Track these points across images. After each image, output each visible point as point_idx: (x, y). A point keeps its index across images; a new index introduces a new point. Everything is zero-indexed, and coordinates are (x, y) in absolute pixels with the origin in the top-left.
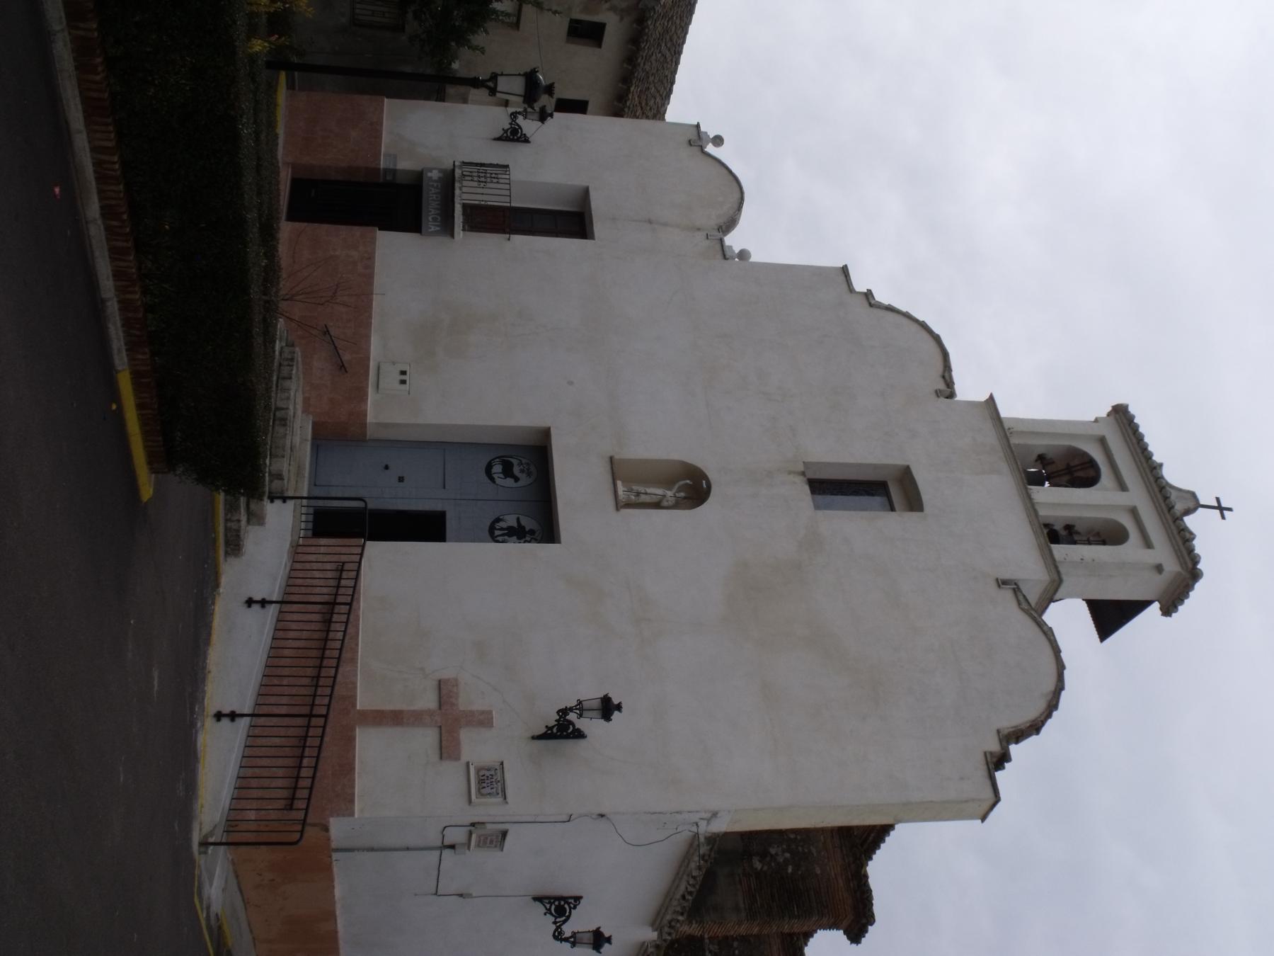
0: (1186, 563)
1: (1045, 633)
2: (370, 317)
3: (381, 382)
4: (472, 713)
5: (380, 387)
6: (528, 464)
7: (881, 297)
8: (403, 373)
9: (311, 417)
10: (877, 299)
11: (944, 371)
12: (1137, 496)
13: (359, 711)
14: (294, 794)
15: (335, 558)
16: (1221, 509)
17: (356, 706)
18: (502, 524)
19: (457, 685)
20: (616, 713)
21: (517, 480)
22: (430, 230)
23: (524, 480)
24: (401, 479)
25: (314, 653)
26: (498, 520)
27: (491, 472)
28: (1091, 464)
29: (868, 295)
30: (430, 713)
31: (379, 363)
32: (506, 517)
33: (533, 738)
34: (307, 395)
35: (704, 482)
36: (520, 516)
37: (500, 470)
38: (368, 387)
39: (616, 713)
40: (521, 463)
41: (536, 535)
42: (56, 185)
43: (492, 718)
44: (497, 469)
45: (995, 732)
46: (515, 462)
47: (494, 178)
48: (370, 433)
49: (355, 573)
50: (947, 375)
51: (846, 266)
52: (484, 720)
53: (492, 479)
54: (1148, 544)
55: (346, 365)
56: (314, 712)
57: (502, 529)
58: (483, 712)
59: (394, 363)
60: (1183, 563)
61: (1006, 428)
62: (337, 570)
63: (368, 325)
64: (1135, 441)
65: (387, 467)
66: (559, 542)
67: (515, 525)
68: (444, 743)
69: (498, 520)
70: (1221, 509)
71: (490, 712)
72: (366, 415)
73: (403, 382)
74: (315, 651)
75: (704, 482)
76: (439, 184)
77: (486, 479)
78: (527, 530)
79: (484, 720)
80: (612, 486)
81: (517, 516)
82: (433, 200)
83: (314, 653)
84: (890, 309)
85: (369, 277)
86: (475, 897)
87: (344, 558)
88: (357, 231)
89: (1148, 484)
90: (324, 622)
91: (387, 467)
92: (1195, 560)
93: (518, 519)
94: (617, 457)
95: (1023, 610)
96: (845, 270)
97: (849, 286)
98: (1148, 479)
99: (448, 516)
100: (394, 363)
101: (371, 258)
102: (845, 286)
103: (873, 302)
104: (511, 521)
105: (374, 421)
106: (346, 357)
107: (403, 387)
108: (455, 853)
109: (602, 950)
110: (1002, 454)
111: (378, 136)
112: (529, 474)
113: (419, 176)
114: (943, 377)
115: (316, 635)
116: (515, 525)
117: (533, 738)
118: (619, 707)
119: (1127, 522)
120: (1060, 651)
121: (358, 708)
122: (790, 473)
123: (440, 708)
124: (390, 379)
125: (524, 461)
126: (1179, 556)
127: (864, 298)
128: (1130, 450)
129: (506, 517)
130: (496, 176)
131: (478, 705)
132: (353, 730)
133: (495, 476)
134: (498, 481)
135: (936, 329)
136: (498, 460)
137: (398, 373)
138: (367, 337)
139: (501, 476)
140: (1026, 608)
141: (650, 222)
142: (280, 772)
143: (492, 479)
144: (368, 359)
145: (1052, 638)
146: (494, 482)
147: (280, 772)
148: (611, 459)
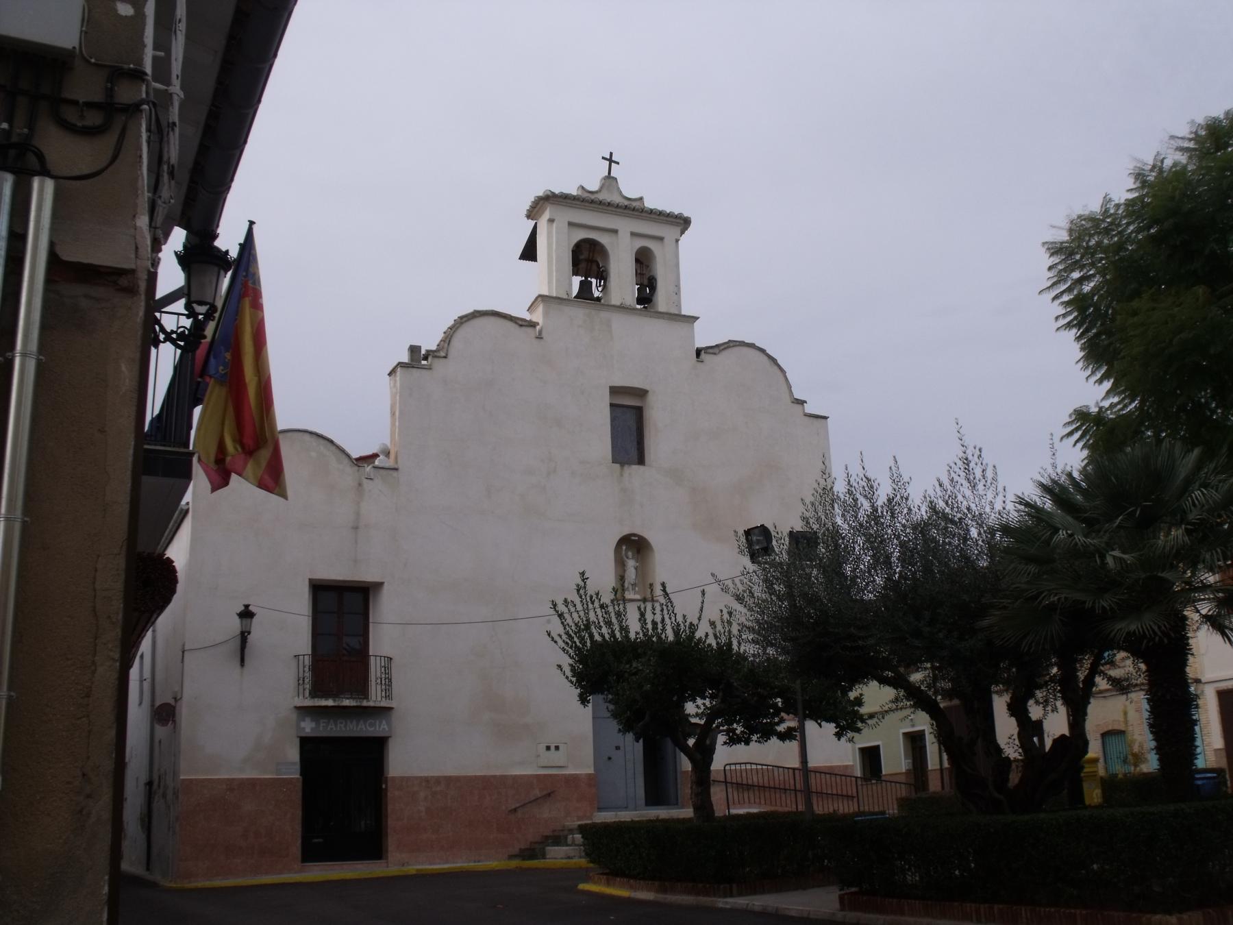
2: (495, 777)
3: (558, 765)
8: (548, 748)
9: (595, 814)
11: (516, 323)
12: (625, 226)
14: (845, 796)
20: (250, 608)
22: (387, 729)
24: (618, 748)
25: (767, 794)
34: (575, 819)
39: (250, 608)
42: (185, 344)
45: (792, 404)
47: (304, 681)
49: (897, 784)
50: (520, 323)
55: (545, 792)
56: (797, 792)
57: (1110, 679)
59: (539, 756)
62: (785, 793)
65: (610, 758)
72: (590, 774)
73: (557, 748)
74: (766, 793)
76: (322, 721)
82: (345, 726)
83: (767, 794)
85: (450, 780)
86: (1206, 683)
88: (392, 794)
89: (614, 213)
90: (748, 790)
95: (719, 353)
101: (427, 780)
105: (592, 768)
106: (537, 793)
107: (560, 748)
108: (390, 737)
109: (298, 739)
111: (252, 783)
113: (305, 742)
114: (521, 326)
115: (757, 793)
122: (622, 475)
126: (672, 223)
128: (582, 208)
130: (301, 679)
135: (470, 310)
137: (548, 752)
138: (515, 778)
141: (356, 528)
142: (741, 795)
144: (538, 776)
145: (738, 343)
147: (741, 795)
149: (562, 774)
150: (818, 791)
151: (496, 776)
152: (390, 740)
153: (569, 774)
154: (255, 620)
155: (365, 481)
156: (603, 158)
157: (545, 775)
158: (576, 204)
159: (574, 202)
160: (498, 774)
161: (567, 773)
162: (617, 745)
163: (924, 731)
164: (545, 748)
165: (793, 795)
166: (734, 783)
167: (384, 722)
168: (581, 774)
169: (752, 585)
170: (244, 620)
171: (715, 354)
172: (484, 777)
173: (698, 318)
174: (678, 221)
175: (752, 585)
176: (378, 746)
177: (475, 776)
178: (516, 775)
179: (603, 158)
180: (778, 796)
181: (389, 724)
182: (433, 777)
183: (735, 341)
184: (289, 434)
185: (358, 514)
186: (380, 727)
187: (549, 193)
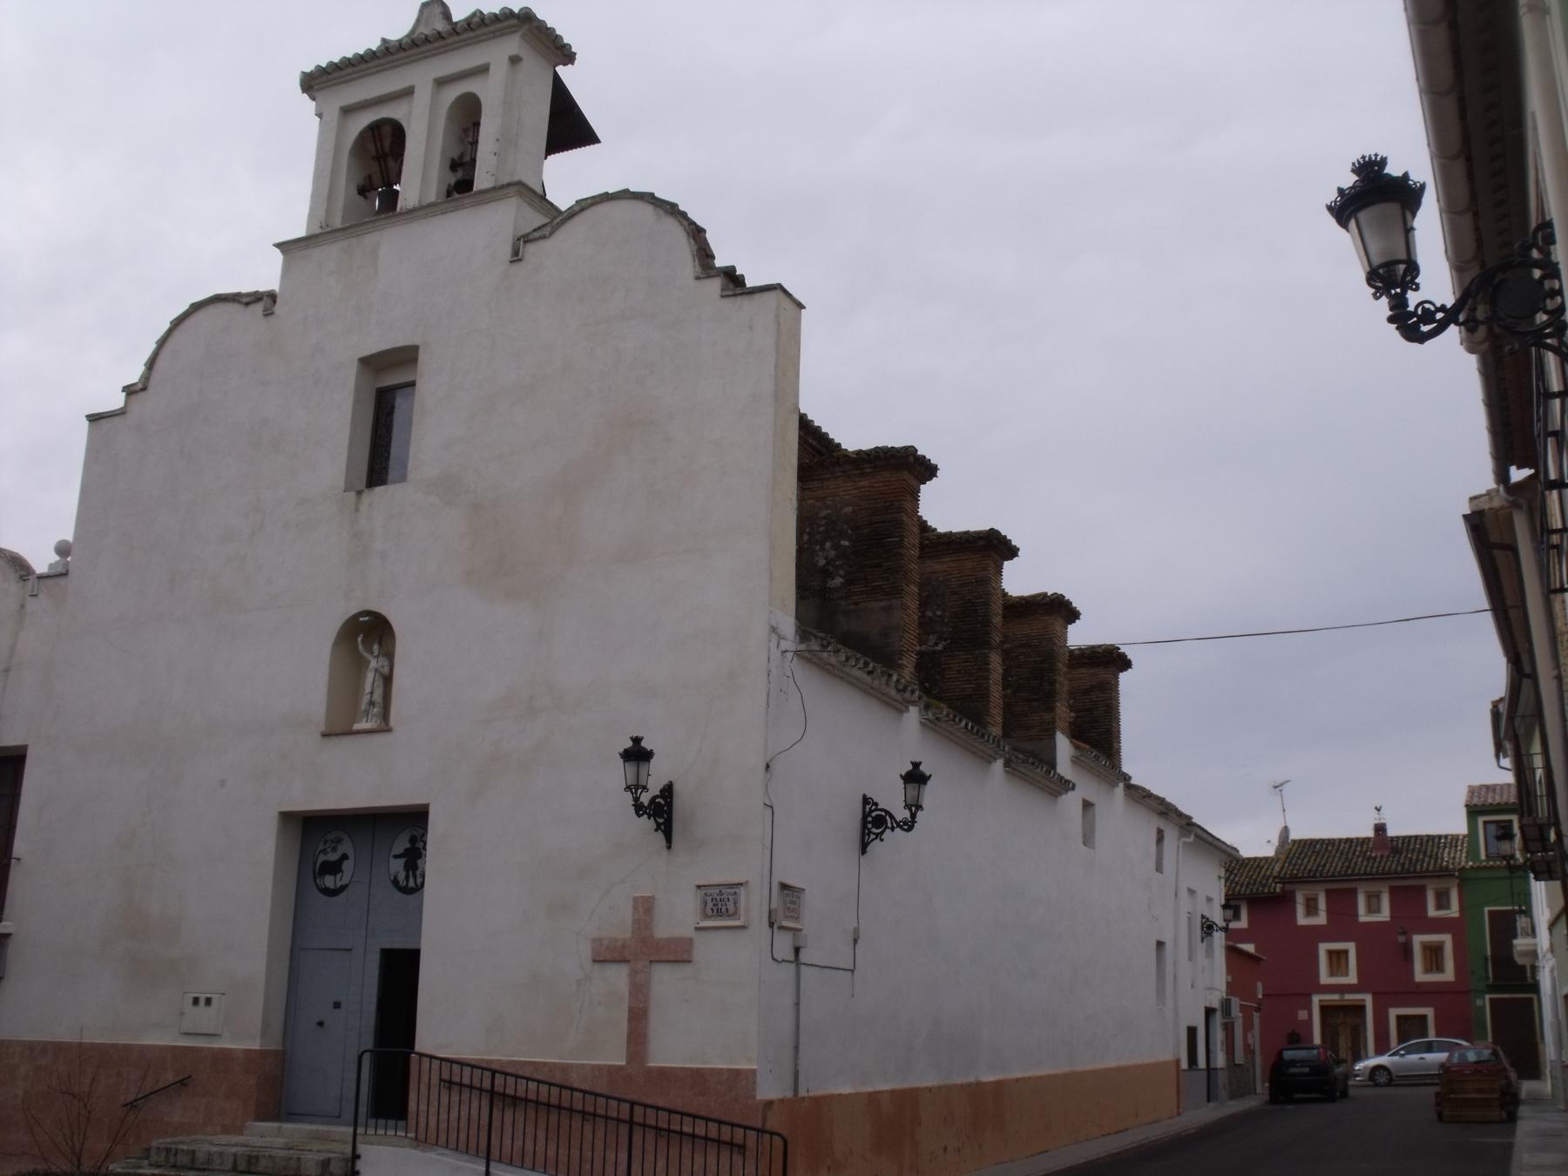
1: (583, 210)
2: (115, 1046)
4: (636, 922)
5: (211, 1032)
6: (325, 842)
7: (134, 375)
8: (196, 1001)
11: (239, 302)
12: (421, 76)
13: (627, 1063)
14: (726, 1143)
15: (435, 1091)
18: (402, 877)
19: (600, 940)
20: (643, 744)
21: (344, 857)
23: (346, 847)
24: (337, 1005)
25: (553, 1118)
26: (395, 882)
27: (334, 890)
28: (375, 129)
29: (130, 391)
30: (633, 974)
31: (180, 1033)
32: (393, 871)
33: (669, 847)
35: (361, 619)
36: (392, 854)
37: (332, 878)
38: (213, 1048)
39: (643, 744)
40: (324, 851)
43: (643, 897)
44: (329, 881)
46: (322, 858)
48: (274, 1045)
50: (245, 300)
52: (645, 907)
53: (343, 888)
54: (483, 70)
57: (407, 878)
58: (635, 908)
59: (182, 1014)
60: (510, 31)
62: (450, 1089)
64: (350, 70)
65: (321, 1024)
67: (402, 861)
68: (671, 958)
69: (395, 882)
71: (636, 899)
73: (208, 1001)
75: (361, 619)
77: (343, 895)
78: (408, 845)
80: (359, 736)
81: (391, 859)
83: (553, 1118)
84: (151, 364)
85: (58, 1048)
87: (435, 1080)
91: (321, 1024)
92: (507, 14)
93: (396, 857)
94: (323, 728)
95: (552, 233)
96: (94, 419)
99: (388, 946)
100: (182, 1014)
101: (31, 1046)
102: (116, 420)
103: (140, 386)
104: (397, 866)
106: (170, 1077)
107: (215, 1003)
110: (354, 240)
112: (339, 841)
114: (247, 304)
115: (531, 1114)
116: (402, 861)
117: (669, 847)
118: (637, 740)
119: (452, 93)
120: (607, 193)
121: (624, 1063)
124: (205, 1019)
125: (321, 847)
127: (133, 397)
129: (393, 871)
131: (627, 914)
132: (651, 1070)
133: (339, 884)
134: (345, 881)
135: (184, 307)
136: (318, 881)
138: (144, 1049)
139: (339, 876)
140: (549, 229)
142: (699, 1159)
143: (343, 888)
145: (589, 201)
146: (347, 886)
147: (699, 1159)
148: (324, 735)
149: (209, 1049)
150: (735, 1141)
151: (117, 1044)
158: (335, 79)
159: (343, 73)
161: (216, 1046)
162: (332, 1006)
164: (191, 1001)
166: (698, 1137)
168: (235, 1050)
169: (991, 738)
170: (910, 786)
175: (991, 738)
182: (39, 1042)
187: (507, 11)
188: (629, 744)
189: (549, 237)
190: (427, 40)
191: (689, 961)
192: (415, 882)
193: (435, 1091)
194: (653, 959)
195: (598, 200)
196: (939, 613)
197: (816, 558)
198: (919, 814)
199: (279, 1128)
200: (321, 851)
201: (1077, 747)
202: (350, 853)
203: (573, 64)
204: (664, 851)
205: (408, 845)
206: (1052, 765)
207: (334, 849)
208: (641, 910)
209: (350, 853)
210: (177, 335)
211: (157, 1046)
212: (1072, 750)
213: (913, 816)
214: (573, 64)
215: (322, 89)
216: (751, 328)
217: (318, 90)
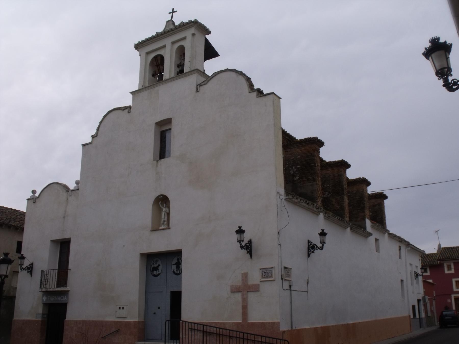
0: (192, 25)
1: (215, 75)
2: (99, 321)
5: (125, 317)
6: (153, 262)
7: (94, 133)
8: (120, 308)
9: (136, 342)
10: (94, 134)
11: (121, 110)
12: (167, 41)
13: (242, 321)
15: (187, 331)
16: (173, 12)
17: (241, 322)
21: (159, 265)
22: (66, 300)
23: (159, 263)
24: (159, 308)
26: (174, 272)
28: (156, 58)
29: (93, 137)
30: (243, 295)
32: (173, 269)
33: (251, 258)
35: (160, 197)
36: (172, 264)
37: (156, 271)
38: (125, 321)
39: (242, 228)
40: (153, 264)
41: (179, 258)
43: (244, 273)
44: (155, 272)
45: (250, 93)
46: (153, 266)
48: (144, 321)
51: (82, 145)
52: (245, 276)
53: (159, 274)
54: (185, 38)
57: (177, 271)
58: (242, 276)
61: (142, 88)
63: (102, 322)
66: (181, 250)
67: (175, 266)
69: (174, 272)
70: (173, 12)
73: (123, 308)
75: (160, 197)
77: (159, 276)
79: (245, 276)
81: (172, 265)
84: (98, 129)
88: (66, 327)
91: (155, 313)
92: (190, 22)
94: (151, 229)
95: (207, 83)
96: (84, 145)
97: (90, 144)
98: (161, 38)
99: (172, 290)
100: (116, 312)
102: (89, 145)
103: (95, 135)
106: (114, 330)
107: (125, 308)
110: (152, 90)
112: (157, 261)
113: (45, 304)
114: (123, 110)
116: (175, 266)
117: (251, 258)
118: (240, 227)
120: (222, 70)
121: (241, 322)
122: (157, 166)
123: (241, 292)
124: (122, 313)
126: (187, 28)
127: (94, 139)
133: (158, 273)
134: (159, 272)
139: (158, 271)
140: (206, 82)
141: (64, 217)
143: (159, 274)
144: (114, 322)
145: (217, 73)
148: (151, 231)
149: (124, 321)
151: (99, 321)
152: (68, 304)
153: (127, 321)
154: (25, 259)
155: (69, 197)
156: (173, 9)
157: (118, 321)
160: (100, 320)
163: (454, 296)
165: (201, 334)
167: (66, 297)
171: (205, 84)
172: (95, 321)
173: (130, 93)
174: (190, 25)
176: (64, 306)
177: (92, 321)
178: (106, 321)
179: (173, 9)
180: (193, 333)
181: (67, 297)
183: (215, 73)
184: (51, 186)
185: (65, 211)
186: (64, 299)
188: (238, 228)
189: (206, 84)
190: (168, 31)
191: (258, 291)
192: (179, 272)
193: (187, 331)
194: (248, 291)
195: (219, 72)
196: (328, 185)
197: (291, 171)
198: (325, 245)
199: (145, 343)
200: (152, 264)
201: (372, 223)
202: (161, 264)
203: (210, 34)
204: (250, 259)
205: (177, 261)
206: (365, 228)
207: (156, 263)
208: (244, 277)
209: (161, 264)
210: (105, 120)
211: (110, 321)
212: (371, 223)
213: (323, 245)
214: (210, 34)
215: (140, 48)
216: (266, 106)
217: (139, 48)
